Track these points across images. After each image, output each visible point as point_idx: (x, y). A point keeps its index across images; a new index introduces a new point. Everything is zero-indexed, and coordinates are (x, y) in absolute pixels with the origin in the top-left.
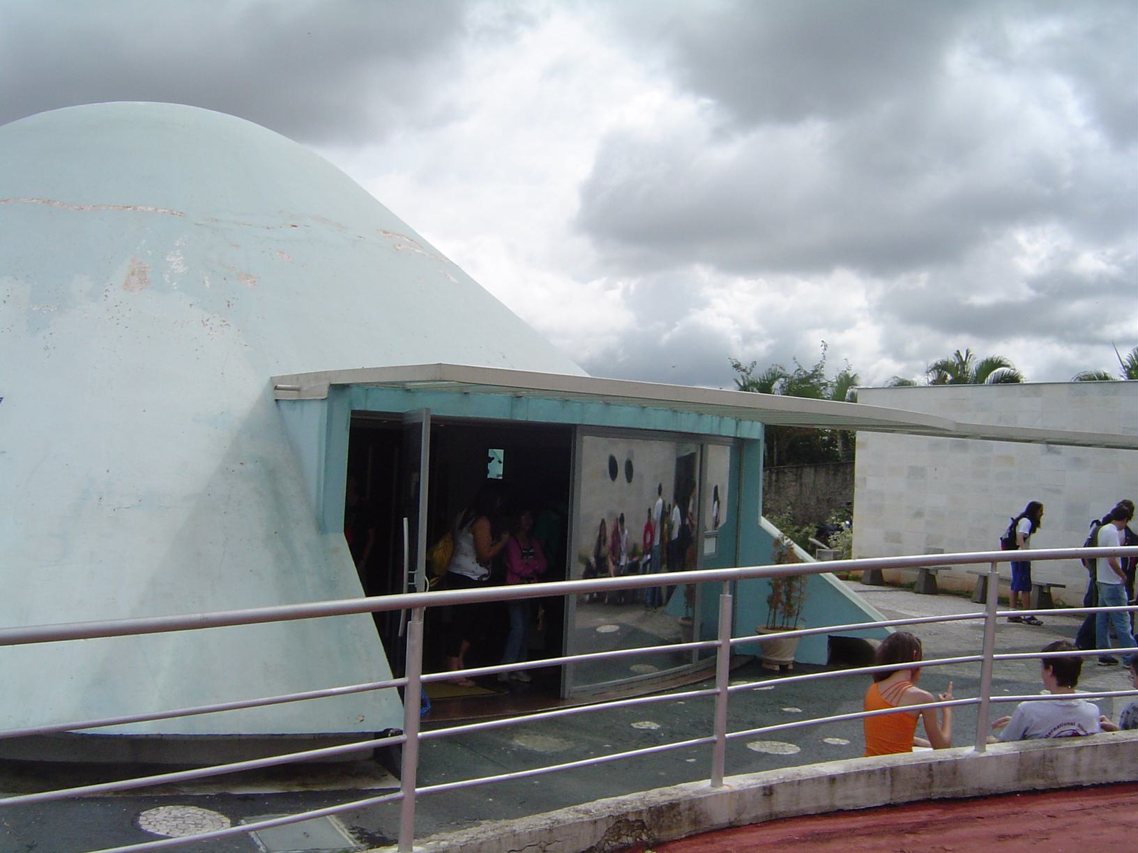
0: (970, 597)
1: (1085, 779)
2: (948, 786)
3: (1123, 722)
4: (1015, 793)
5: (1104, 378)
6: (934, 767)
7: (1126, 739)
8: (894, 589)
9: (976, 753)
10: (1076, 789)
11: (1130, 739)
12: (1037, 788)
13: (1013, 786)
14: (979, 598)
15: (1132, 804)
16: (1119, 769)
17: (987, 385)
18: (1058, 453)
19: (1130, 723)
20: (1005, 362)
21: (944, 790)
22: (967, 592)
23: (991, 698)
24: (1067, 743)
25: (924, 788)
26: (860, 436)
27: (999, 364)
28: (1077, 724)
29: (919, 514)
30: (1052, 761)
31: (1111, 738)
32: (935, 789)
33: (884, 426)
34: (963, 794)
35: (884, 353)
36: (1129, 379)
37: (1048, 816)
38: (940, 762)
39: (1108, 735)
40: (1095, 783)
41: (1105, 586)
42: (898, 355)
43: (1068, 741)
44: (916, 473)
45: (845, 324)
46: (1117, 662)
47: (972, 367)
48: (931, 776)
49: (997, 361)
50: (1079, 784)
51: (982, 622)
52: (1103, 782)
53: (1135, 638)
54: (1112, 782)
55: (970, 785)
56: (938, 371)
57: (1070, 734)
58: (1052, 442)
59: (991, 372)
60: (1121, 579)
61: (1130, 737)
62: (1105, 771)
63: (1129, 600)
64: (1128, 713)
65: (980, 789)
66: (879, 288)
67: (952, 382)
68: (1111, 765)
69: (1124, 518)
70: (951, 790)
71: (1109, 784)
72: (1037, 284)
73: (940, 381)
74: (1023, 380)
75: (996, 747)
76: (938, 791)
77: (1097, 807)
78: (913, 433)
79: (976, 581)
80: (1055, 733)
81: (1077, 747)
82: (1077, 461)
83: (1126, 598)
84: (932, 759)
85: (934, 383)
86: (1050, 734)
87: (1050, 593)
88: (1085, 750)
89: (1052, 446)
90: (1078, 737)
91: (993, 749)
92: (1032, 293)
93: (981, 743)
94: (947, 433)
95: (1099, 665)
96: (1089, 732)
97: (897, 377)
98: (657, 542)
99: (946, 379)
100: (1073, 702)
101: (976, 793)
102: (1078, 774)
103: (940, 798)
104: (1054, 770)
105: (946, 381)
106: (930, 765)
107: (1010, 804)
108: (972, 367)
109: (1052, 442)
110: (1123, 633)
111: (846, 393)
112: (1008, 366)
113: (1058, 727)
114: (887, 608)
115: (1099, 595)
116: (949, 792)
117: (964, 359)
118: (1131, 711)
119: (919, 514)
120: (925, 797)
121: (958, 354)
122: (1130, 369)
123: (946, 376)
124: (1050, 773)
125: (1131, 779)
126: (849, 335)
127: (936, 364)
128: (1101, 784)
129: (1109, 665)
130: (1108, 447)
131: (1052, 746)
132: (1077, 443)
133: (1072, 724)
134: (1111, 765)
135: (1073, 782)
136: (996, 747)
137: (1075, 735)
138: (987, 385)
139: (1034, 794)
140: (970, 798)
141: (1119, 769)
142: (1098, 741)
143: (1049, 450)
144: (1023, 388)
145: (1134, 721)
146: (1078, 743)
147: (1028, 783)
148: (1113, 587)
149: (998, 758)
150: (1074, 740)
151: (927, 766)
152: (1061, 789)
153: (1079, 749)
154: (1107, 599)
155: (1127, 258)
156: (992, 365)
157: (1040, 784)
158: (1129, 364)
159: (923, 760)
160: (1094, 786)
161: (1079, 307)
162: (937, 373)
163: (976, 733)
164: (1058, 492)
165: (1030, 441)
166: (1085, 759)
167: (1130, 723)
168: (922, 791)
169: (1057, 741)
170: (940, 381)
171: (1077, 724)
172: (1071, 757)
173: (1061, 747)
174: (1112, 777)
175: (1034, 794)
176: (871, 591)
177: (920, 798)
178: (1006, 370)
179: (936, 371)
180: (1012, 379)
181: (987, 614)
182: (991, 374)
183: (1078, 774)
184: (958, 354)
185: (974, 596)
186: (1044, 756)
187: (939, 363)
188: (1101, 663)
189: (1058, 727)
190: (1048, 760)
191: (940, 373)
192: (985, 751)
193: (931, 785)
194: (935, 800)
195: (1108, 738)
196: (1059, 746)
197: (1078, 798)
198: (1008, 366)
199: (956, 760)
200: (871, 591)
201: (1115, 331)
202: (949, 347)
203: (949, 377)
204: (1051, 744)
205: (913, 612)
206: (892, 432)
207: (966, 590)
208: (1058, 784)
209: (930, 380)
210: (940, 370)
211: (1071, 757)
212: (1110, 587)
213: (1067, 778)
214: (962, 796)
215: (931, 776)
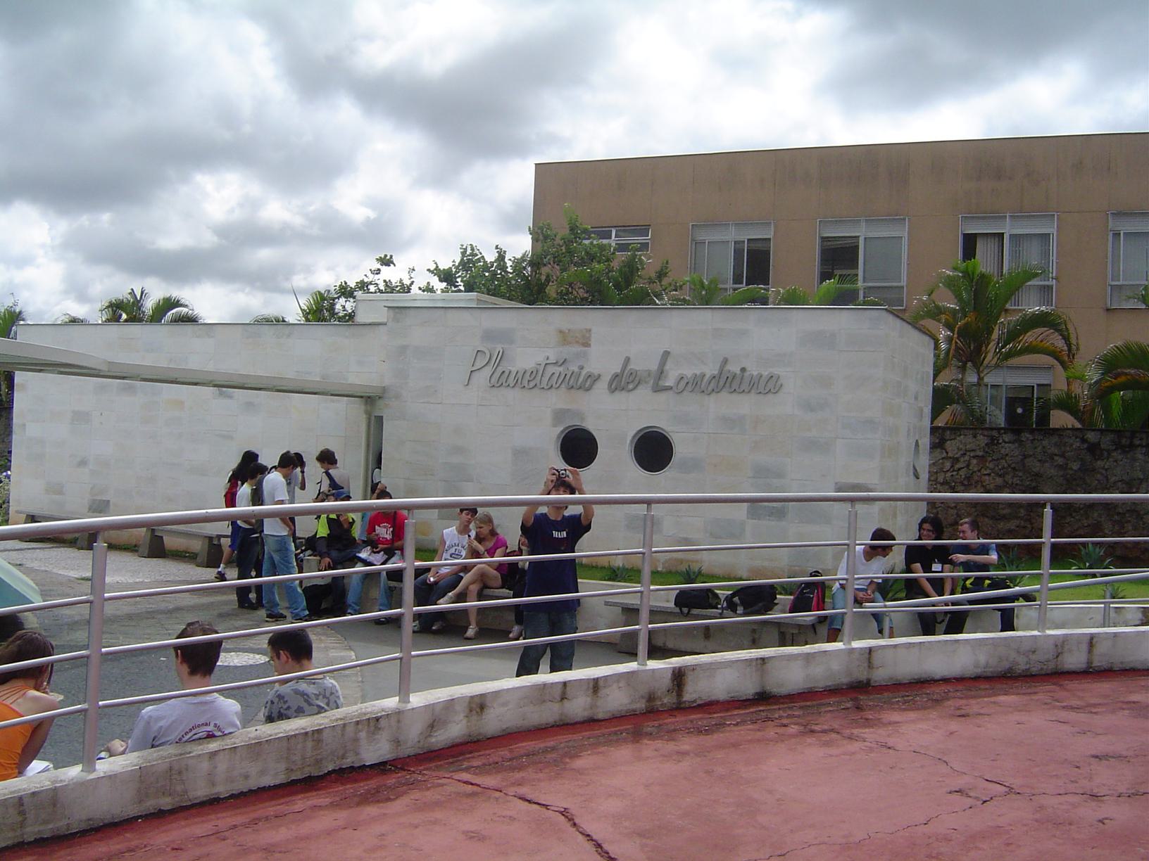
0: (137, 551)
1: (222, 790)
2: (45, 822)
3: (266, 714)
4: (136, 818)
5: (280, 321)
6: (25, 800)
7: (271, 736)
8: (55, 545)
9: (84, 774)
10: (214, 803)
11: (276, 734)
12: (162, 808)
13: (132, 811)
14: (147, 551)
15: (276, 817)
16: (262, 773)
17: (164, 324)
18: (230, 397)
19: (275, 715)
20: (182, 301)
21: (42, 828)
22: (136, 546)
23: (100, 703)
24: (200, 747)
25: (13, 830)
26: (19, 377)
27: (177, 304)
28: (212, 725)
29: (83, 463)
30: (180, 773)
31: (252, 735)
32: (28, 829)
33: (24, 364)
34: (68, 830)
35: (66, 292)
36: (306, 321)
37: (173, 849)
38: (34, 793)
39: (248, 733)
40: (234, 792)
41: (272, 538)
42: (82, 297)
43: (201, 745)
44: (80, 417)
45: (23, 261)
46: (285, 617)
47: (149, 305)
48: (22, 813)
49: (174, 300)
50: (216, 796)
51: (85, 610)
52: (245, 791)
53: (303, 591)
54: (255, 788)
55: (77, 817)
56: (112, 310)
57: (205, 736)
58: (224, 385)
59: (169, 312)
60: (288, 529)
61: (276, 731)
62: (247, 777)
63: (296, 550)
64: (272, 702)
65: (89, 820)
66: (63, 226)
67: (126, 321)
68: (253, 768)
69: (289, 466)
70: (51, 826)
71: (251, 791)
72: (224, 231)
73: (115, 319)
74: (201, 321)
75: (110, 763)
76: (32, 831)
77: (235, 826)
78: (62, 373)
79: (143, 534)
80: (187, 737)
81: (212, 752)
82: (250, 406)
83: (294, 549)
84: (24, 790)
85: (108, 320)
86: (180, 739)
87: (220, 545)
88: (222, 754)
89: (224, 389)
90: (214, 739)
91: (105, 766)
92: (215, 239)
93: (89, 761)
94: (93, 372)
95: (267, 621)
96: (226, 732)
97: (68, 314)
98: (1019, 348)
99: (120, 318)
100: (208, 698)
101: (84, 826)
102: (213, 784)
103: (36, 839)
104: (184, 784)
105: (121, 320)
106: (20, 798)
107: (128, 835)
108: (149, 305)
109: (224, 385)
110: (291, 587)
111: (11, 330)
112: (186, 306)
113: (191, 730)
114: (43, 569)
115: (265, 547)
116: (47, 830)
117: (139, 299)
118: (276, 700)
119: (83, 463)
120: (16, 841)
121: (132, 293)
122: (308, 313)
123: (121, 315)
124: (179, 788)
125: (278, 782)
126: (29, 273)
127: (110, 302)
128: (242, 792)
129: (277, 621)
130: (332, 395)
131: (181, 754)
132: (246, 386)
133: (206, 724)
134: (253, 768)
135: (208, 796)
136: (110, 763)
137: (211, 736)
138: (164, 324)
139: (159, 816)
140: (77, 833)
141: (262, 773)
142: (237, 741)
143: (221, 394)
144: (200, 327)
145: (280, 712)
146: (213, 746)
147: (150, 805)
148: (279, 539)
149: (111, 778)
150: (208, 743)
151: (17, 800)
152: (193, 806)
153: (213, 754)
154: (273, 551)
155: (312, 208)
156: (170, 304)
157: (166, 803)
158: (306, 308)
159: (11, 793)
160: (232, 796)
161: (265, 255)
162: (111, 312)
163: (83, 750)
164: (231, 438)
165: (196, 384)
166: (222, 765)
167: (275, 715)
168: (10, 834)
169: (189, 747)
170: (115, 319)
171: (212, 725)
172: (205, 765)
173: (191, 755)
174: (254, 783)
175: (159, 816)
176: (29, 549)
177: (10, 843)
178: (184, 310)
179: (110, 309)
180: (190, 320)
181: (91, 598)
182: (169, 314)
183: (213, 784)
184: (132, 293)
185: (140, 550)
186: (171, 769)
187: (114, 301)
188: (268, 619)
189: (191, 730)
190: (174, 772)
191: (114, 312)
192: (95, 770)
193: (22, 824)
194: (30, 843)
195: (249, 735)
196: (190, 753)
197: (213, 817)
198: (186, 306)
199: (55, 787)
200: (29, 549)
201: (299, 281)
202: (120, 286)
203: (124, 316)
204: (180, 752)
205: (72, 572)
206: (40, 371)
207: (134, 544)
208: (190, 800)
209: (104, 319)
210: (115, 308)
211: (205, 765)
212: (276, 538)
213: (201, 791)
214: (67, 833)
215: (22, 813)
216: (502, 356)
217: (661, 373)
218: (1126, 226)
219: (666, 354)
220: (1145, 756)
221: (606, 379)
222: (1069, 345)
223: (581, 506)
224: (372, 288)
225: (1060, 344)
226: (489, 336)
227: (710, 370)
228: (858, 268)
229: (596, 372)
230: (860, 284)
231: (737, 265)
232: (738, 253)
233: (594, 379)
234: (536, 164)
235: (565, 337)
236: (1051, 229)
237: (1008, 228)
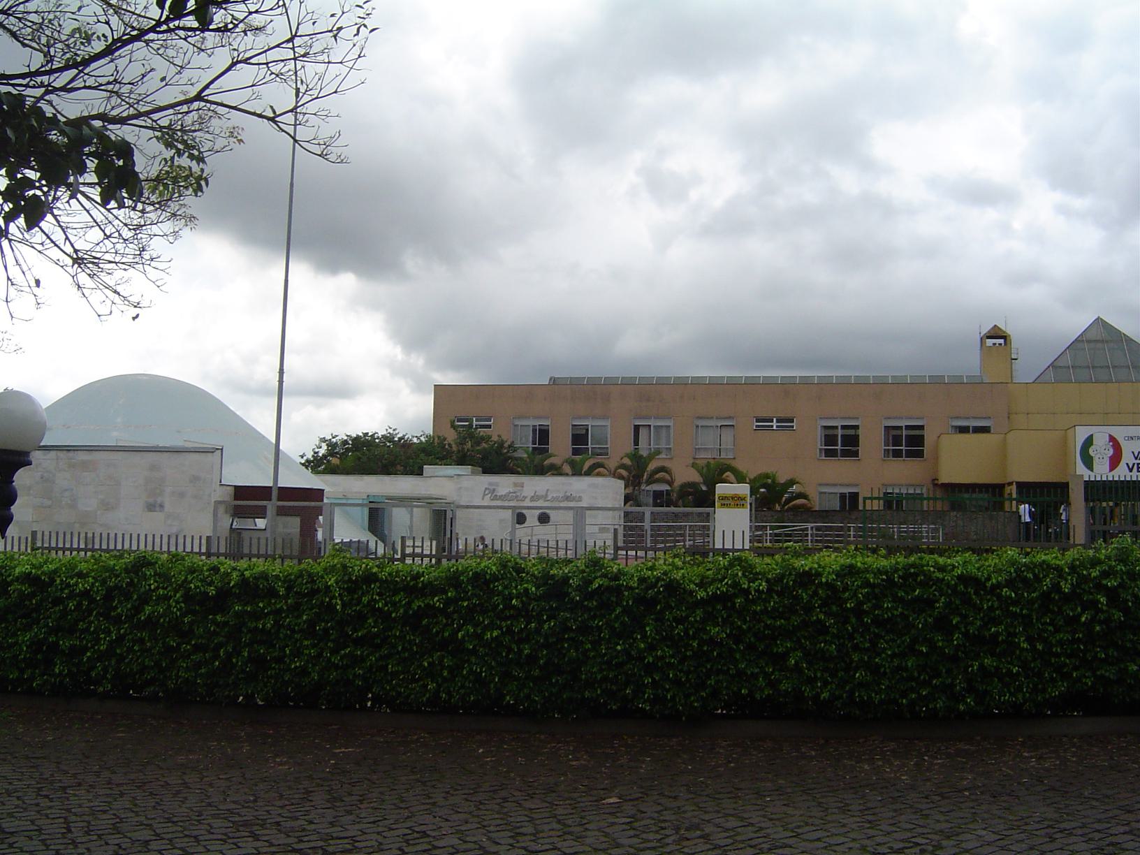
216: (494, 490)
217: (547, 495)
218: (701, 423)
219: (548, 490)
220: (1054, 414)
221: (529, 498)
222: (672, 479)
223: (136, 549)
224: (883, 552)
225: (669, 478)
226: (490, 484)
227: (561, 495)
228: (573, 435)
229: (526, 495)
230: (590, 446)
231: (534, 438)
232: (534, 431)
233: (525, 497)
234: (435, 385)
235: (515, 485)
236: (671, 424)
237: (652, 423)
